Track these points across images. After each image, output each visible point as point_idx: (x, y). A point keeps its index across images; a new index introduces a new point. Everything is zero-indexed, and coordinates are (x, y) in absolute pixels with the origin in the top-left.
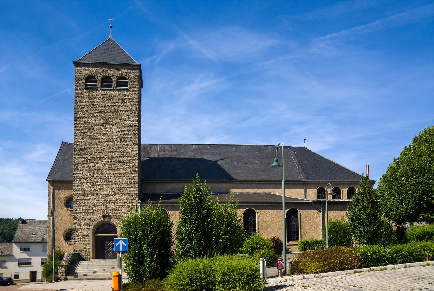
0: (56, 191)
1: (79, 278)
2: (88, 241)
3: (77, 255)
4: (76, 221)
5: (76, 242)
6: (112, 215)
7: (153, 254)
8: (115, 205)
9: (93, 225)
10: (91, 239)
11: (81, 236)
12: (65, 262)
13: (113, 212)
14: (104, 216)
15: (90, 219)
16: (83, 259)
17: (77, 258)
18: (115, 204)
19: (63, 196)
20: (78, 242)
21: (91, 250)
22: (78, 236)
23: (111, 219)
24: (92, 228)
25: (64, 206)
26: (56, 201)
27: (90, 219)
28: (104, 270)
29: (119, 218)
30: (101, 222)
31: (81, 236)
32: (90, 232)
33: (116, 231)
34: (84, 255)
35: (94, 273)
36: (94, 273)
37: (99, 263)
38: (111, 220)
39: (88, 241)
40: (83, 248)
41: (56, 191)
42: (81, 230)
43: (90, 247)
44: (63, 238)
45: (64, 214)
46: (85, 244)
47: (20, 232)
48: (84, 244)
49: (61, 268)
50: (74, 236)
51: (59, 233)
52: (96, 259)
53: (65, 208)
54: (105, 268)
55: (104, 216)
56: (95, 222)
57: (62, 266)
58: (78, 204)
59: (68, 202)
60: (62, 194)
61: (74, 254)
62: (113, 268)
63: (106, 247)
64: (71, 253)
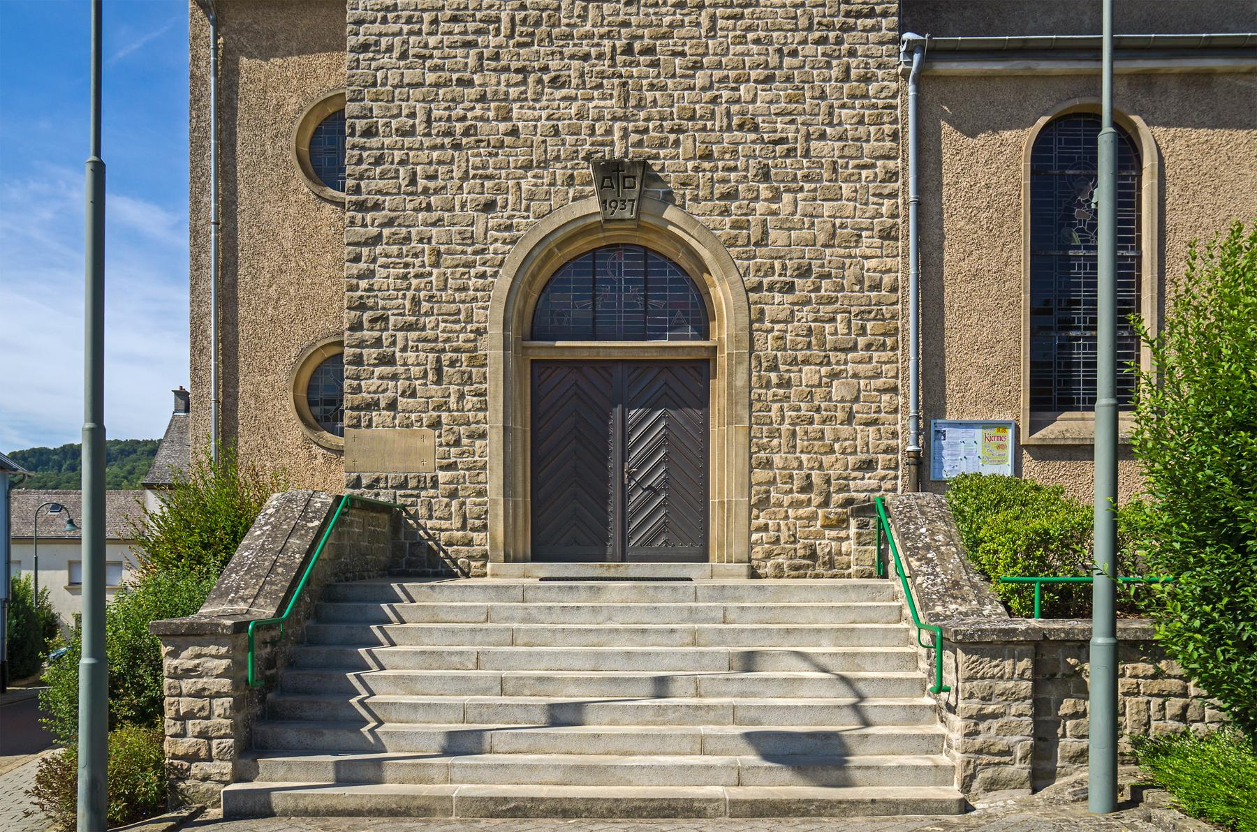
0: (244, 61)
1: (389, 790)
2: (470, 401)
3: (383, 524)
4: (372, 223)
5: (372, 406)
6: (673, 165)
7: (454, 562)
8: (701, 78)
9: (516, 256)
10: (494, 387)
11: (413, 360)
12: (245, 593)
13: (686, 142)
14: (611, 174)
15: (489, 207)
16: (428, 564)
17: (379, 554)
18: (697, 66)
19: (292, 103)
20: (392, 406)
21: (494, 481)
22: (388, 360)
23: (668, 198)
24: (503, 282)
25: (299, 172)
26: (242, 134)
27: (489, 207)
28: (661, 686)
29: (731, 196)
30: (584, 229)
31: (413, 360)
32: (492, 317)
33: (699, 316)
34: (438, 523)
35: (562, 715)
36: (562, 715)
37: (581, 600)
38: (670, 213)
39: (470, 401)
40: (427, 466)
41: (244, 61)
42: (416, 302)
43: (491, 450)
44: (289, 404)
45: (299, 231)
46: (446, 443)
47: (177, 447)
48: (436, 424)
49: (185, 660)
50: (358, 361)
51: (264, 371)
52: (536, 557)
53: (302, 186)
54: (666, 656)
55: (611, 174)
56: (532, 230)
57: (201, 634)
58: (393, 78)
59: (325, 150)
60: (285, 87)
61: (353, 508)
62: (749, 661)
63: (614, 463)
64: (323, 500)
